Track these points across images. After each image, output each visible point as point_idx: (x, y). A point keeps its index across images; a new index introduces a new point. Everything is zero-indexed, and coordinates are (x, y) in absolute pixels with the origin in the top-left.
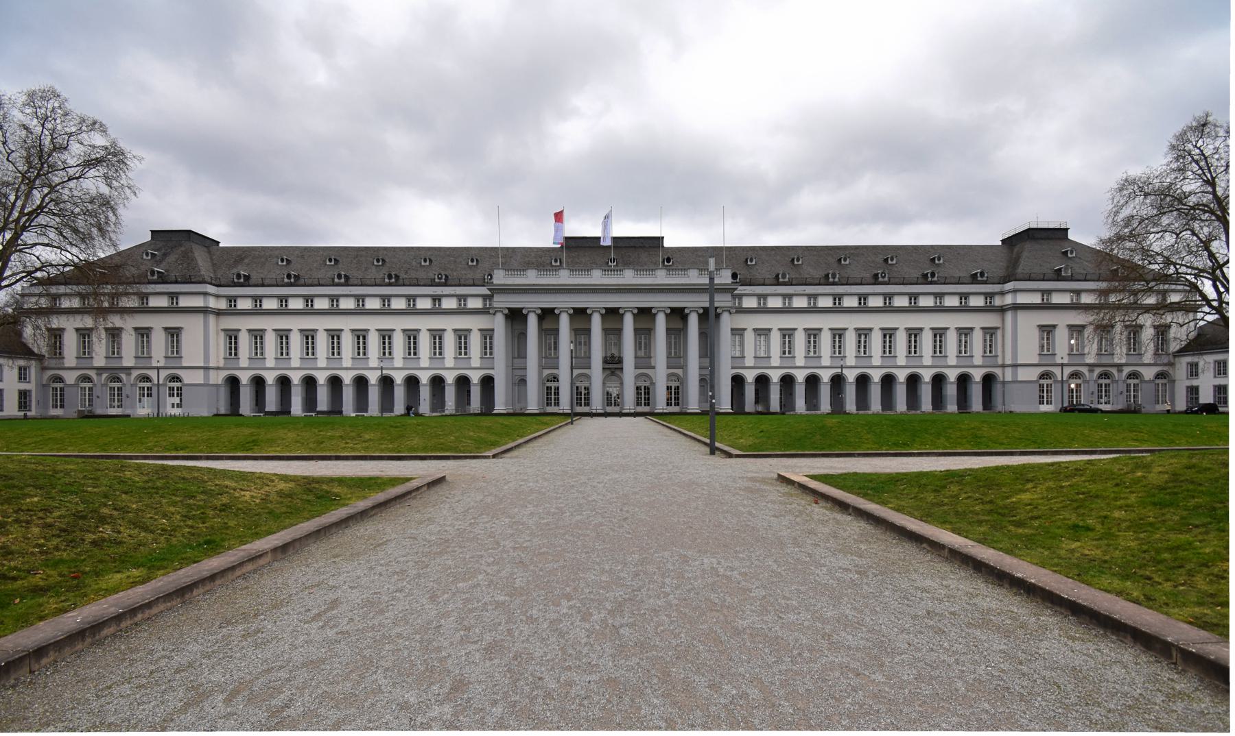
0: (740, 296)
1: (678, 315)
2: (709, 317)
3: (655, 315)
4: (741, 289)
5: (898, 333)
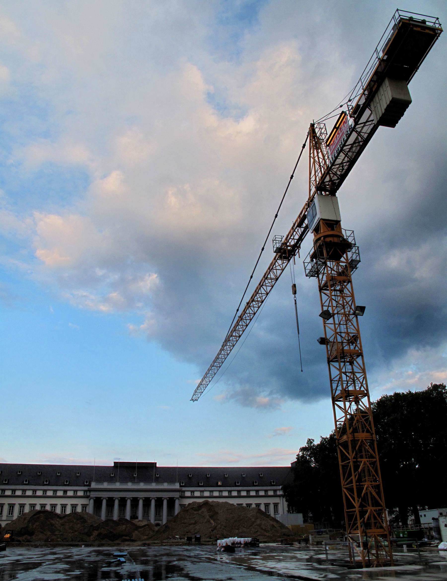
0: (184, 491)
1: (159, 501)
2: (171, 502)
3: (151, 500)
4: (184, 489)
5: (26, 506)
